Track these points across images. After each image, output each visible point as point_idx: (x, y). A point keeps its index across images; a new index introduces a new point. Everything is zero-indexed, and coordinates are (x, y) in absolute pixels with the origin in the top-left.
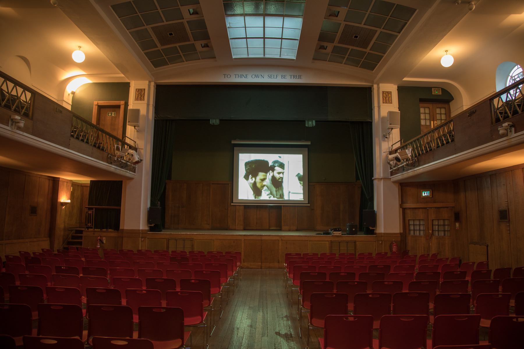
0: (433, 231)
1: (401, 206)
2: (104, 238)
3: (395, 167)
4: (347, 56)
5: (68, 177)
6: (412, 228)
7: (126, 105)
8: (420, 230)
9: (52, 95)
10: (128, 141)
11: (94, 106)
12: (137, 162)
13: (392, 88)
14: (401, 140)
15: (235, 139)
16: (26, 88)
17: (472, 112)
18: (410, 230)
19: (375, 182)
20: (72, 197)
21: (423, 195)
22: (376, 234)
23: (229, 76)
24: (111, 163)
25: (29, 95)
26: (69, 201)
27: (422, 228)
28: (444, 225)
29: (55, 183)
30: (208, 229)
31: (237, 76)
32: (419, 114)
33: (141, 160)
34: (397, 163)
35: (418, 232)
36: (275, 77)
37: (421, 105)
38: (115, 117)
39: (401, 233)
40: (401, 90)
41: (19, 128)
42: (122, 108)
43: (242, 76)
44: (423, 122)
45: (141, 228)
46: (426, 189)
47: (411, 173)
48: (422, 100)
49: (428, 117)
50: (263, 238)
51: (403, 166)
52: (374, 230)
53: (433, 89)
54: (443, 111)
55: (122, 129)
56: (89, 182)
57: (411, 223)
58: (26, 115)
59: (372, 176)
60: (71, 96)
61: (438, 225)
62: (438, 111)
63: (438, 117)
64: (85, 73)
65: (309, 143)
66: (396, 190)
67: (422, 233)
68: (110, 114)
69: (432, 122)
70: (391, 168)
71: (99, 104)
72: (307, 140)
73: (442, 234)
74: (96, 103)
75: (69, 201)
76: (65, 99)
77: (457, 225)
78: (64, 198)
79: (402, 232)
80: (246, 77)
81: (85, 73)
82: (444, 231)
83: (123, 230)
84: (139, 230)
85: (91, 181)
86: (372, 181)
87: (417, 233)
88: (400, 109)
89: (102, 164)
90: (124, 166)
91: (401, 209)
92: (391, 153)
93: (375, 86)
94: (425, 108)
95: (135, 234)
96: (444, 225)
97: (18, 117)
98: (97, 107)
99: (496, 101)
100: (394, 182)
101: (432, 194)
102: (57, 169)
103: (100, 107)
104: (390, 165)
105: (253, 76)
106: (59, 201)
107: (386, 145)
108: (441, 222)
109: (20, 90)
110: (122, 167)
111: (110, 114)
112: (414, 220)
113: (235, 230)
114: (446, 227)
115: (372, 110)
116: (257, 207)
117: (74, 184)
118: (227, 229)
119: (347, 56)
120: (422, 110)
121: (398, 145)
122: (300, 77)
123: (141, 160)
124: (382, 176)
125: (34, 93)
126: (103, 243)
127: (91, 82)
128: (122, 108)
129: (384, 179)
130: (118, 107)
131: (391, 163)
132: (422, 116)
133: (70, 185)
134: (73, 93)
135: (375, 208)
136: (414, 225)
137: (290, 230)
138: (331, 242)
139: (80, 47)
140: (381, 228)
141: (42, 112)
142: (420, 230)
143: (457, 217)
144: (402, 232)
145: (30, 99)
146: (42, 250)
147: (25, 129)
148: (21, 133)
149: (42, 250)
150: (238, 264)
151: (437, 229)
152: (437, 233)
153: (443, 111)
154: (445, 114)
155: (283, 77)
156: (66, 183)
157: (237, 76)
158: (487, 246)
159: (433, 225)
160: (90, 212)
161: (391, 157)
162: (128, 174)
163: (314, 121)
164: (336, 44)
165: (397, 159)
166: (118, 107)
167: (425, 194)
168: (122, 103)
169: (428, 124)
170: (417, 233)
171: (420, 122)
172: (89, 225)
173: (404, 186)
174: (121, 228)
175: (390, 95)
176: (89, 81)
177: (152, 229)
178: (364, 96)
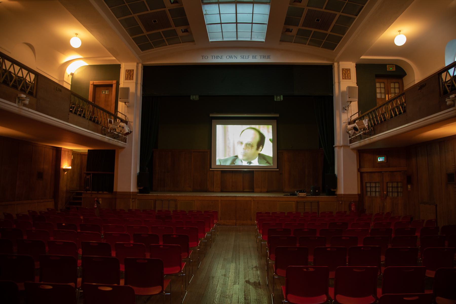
0: (387, 192)
1: (359, 170)
2: (100, 199)
3: (353, 136)
4: (310, 38)
5: (68, 147)
6: (369, 189)
7: (118, 84)
8: (376, 192)
9: (54, 77)
10: (119, 115)
11: (90, 85)
12: (127, 134)
13: (351, 66)
14: (359, 112)
15: (213, 113)
16: (30, 71)
17: (422, 85)
18: (367, 192)
19: (336, 150)
20: (73, 164)
21: (379, 160)
22: (336, 195)
23: (206, 57)
24: (105, 135)
25: (33, 76)
26: (70, 168)
27: (377, 190)
28: (397, 187)
29: (58, 152)
30: (190, 191)
31: (213, 57)
32: (375, 88)
33: (131, 132)
34: (355, 132)
35: (374, 193)
36: (247, 57)
37: (377, 80)
38: (108, 95)
39: (358, 194)
40: (359, 67)
41: (25, 105)
42: (114, 86)
43: (217, 57)
44: (378, 96)
45: (132, 191)
46: (381, 156)
47: (367, 141)
48: (378, 76)
49: (383, 91)
50: (238, 199)
51: (360, 135)
52: (335, 192)
53: (387, 66)
54: (397, 85)
55: (114, 105)
56: (87, 151)
57: (368, 185)
58: (31, 94)
59: (333, 143)
60: (71, 77)
61: (392, 187)
62: (392, 85)
63: (392, 90)
64: (81, 57)
65: (278, 115)
66: (354, 156)
67: (377, 194)
68: (104, 92)
69: (387, 96)
70: (350, 137)
71: (95, 84)
72: (275, 113)
73: (396, 195)
74: (91, 82)
75: (70, 168)
76: (65, 79)
77: (409, 186)
78: (66, 165)
79: (360, 193)
80: (221, 58)
81: (81, 57)
82: (398, 192)
83: (116, 192)
84: (130, 192)
85: (88, 150)
86: (334, 148)
87: (373, 194)
88: (357, 84)
89: (98, 136)
90: (116, 137)
91: (359, 173)
92: (350, 123)
93: (336, 64)
94: (380, 83)
95: (127, 195)
96: (397, 187)
97: (23, 96)
98: (92, 86)
99: (444, 75)
100: (353, 149)
101: (387, 159)
102: (59, 140)
103: (95, 86)
104: (349, 134)
105: (228, 57)
106: (61, 167)
107: (346, 116)
108: (395, 185)
109: (25, 72)
110: (114, 138)
111: (104, 92)
112: (392, 182)
113: (213, 192)
114: (399, 189)
115: (332, 69)
116: (232, 171)
117: (74, 153)
118: (207, 191)
119: (310, 38)
120: (378, 85)
121: (357, 116)
122: (269, 57)
123: (131, 132)
124: (342, 143)
125: (37, 75)
126: (99, 203)
127: (87, 64)
128: (114, 86)
129: (344, 146)
130: (111, 86)
131: (350, 132)
132: (378, 90)
133: (71, 154)
134: (72, 74)
135: (336, 172)
136: (370, 187)
137: (261, 192)
138: (297, 202)
139: (77, 34)
140: (341, 190)
141: (44, 90)
142: (376, 192)
143: (409, 179)
144: (360, 193)
145: (34, 80)
146: (48, 209)
147: (30, 106)
148: (27, 109)
149: (48, 209)
150: (215, 221)
151: (391, 191)
152: (391, 194)
153: (397, 85)
154: (399, 88)
155: (254, 57)
156: (67, 153)
157: (213, 57)
158: (436, 206)
159: (387, 187)
160: (88, 177)
161: (350, 126)
162: (120, 143)
163: (282, 96)
164: (300, 27)
165: (355, 129)
166: (111, 86)
167: (380, 159)
168: (114, 82)
169: (383, 97)
170: (373, 194)
171: (376, 96)
172: (88, 188)
173: (361, 153)
174: (114, 190)
175: (349, 72)
176: (85, 63)
177: (141, 191)
178: (326, 73)
